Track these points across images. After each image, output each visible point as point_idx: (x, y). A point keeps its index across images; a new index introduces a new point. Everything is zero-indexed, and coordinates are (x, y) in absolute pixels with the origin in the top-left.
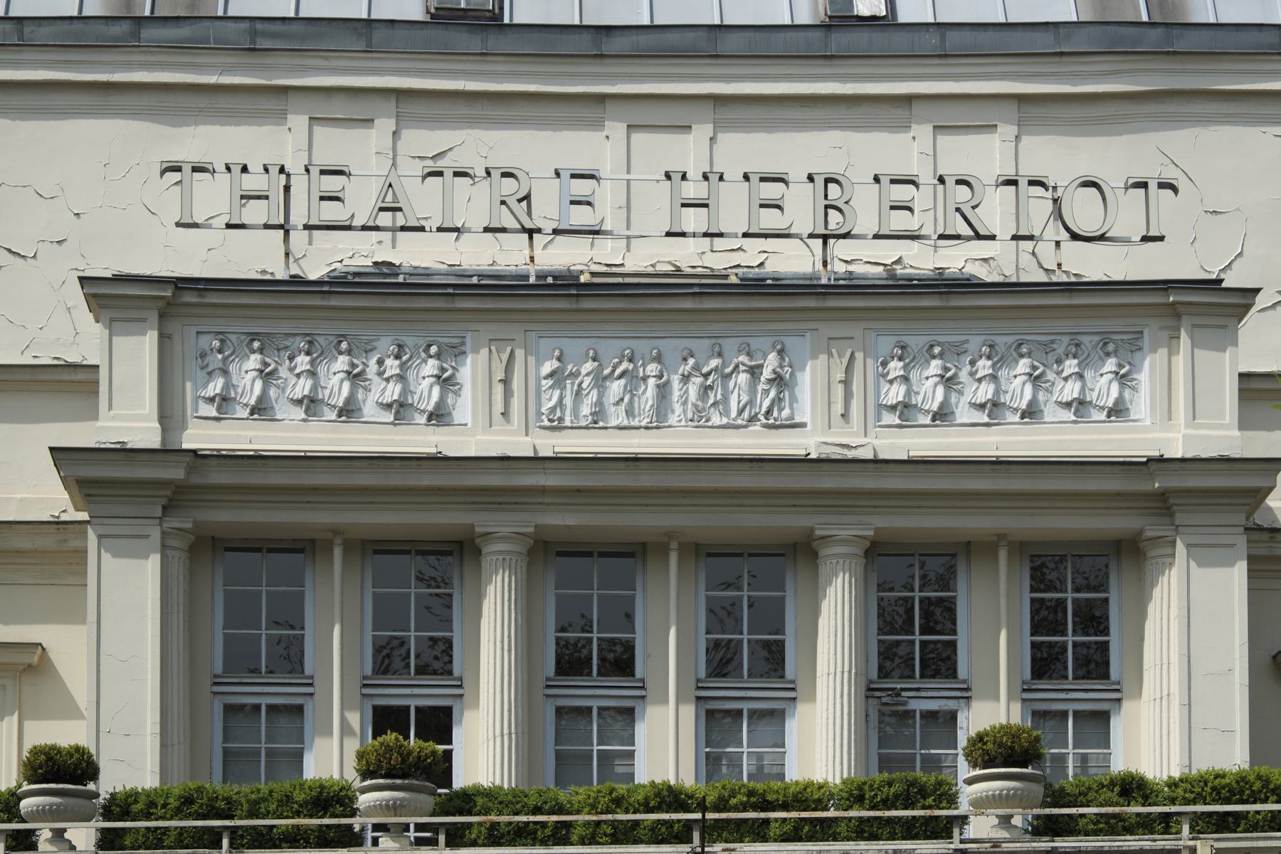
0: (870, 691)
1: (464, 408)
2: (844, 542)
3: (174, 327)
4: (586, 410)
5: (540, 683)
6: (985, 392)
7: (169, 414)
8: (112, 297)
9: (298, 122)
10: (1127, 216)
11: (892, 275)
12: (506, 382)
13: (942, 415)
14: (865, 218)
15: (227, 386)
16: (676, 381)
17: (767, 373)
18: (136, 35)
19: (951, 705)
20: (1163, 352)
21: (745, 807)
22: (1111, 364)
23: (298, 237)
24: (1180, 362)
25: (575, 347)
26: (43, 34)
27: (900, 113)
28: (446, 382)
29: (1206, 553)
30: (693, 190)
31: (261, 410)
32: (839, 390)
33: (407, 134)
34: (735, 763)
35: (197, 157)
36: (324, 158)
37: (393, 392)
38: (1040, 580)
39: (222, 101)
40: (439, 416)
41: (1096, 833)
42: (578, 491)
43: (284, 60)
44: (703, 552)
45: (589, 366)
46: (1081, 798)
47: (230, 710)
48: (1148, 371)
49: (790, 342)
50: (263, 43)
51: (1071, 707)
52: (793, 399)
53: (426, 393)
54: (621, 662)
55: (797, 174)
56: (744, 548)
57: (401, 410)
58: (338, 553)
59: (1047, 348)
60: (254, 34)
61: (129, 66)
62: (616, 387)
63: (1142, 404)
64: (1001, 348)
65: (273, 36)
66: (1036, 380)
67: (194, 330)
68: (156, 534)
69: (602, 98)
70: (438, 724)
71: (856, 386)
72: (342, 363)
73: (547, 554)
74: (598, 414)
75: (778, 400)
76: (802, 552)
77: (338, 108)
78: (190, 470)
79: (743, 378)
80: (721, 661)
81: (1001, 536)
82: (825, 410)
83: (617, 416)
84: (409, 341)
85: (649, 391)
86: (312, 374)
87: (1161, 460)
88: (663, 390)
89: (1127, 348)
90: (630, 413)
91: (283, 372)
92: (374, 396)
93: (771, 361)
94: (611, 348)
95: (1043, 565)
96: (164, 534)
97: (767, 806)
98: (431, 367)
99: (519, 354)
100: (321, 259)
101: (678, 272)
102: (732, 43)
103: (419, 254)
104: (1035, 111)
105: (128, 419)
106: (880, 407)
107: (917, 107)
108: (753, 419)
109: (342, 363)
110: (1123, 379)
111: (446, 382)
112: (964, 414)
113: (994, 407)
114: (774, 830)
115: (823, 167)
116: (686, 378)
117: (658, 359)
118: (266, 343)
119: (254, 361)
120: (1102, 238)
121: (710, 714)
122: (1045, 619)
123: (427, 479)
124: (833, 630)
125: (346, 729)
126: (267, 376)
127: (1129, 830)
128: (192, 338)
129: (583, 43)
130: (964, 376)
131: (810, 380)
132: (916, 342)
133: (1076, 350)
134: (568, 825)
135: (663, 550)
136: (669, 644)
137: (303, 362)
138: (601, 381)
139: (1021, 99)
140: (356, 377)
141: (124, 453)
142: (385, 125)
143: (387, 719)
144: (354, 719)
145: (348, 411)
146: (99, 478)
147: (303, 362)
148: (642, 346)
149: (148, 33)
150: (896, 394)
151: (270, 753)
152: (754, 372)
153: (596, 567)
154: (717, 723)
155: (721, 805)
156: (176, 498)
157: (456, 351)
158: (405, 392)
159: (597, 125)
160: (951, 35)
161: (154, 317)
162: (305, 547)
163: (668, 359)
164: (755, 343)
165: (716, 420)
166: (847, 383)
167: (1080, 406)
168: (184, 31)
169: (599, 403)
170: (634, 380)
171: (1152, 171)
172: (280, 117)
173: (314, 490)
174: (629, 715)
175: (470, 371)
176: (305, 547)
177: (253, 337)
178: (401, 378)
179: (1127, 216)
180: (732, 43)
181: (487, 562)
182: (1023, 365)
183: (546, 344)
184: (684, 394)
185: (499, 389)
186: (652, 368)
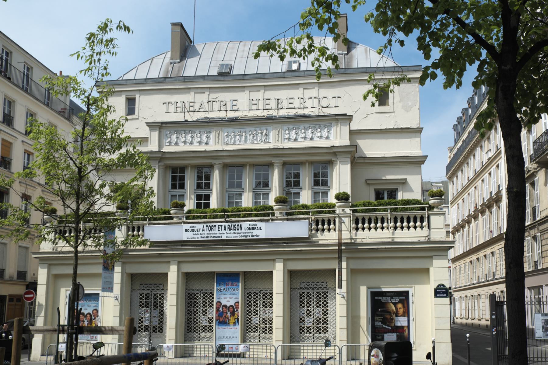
0: (284, 189)
1: (211, 142)
2: (277, 163)
3: (162, 130)
4: (232, 141)
5: (225, 189)
6: (303, 135)
7: (160, 145)
8: (152, 126)
9: (192, 93)
10: (333, 103)
11: (295, 115)
12: (218, 137)
13: (296, 140)
14: (285, 104)
15: (171, 140)
16: (248, 136)
17: (264, 134)
19: (299, 191)
20: (335, 127)
21: (236, 212)
22: (326, 129)
23: (187, 113)
24: (339, 129)
25: (230, 130)
26: (238, 78)
27: (297, 86)
28: (208, 138)
29: (343, 163)
30: (254, 102)
31: (176, 144)
32: (277, 136)
33: (211, 95)
34: (319, 201)
35: (169, 101)
36: (266, 97)
37: (199, 140)
39: (179, 91)
40: (207, 144)
41: (298, 215)
42: (230, 156)
43: (189, 83)
44: (253, 165)
45: (233, 134)
46: (295, 209)
47: (172, 195)
48: (333, 130)
49: (268, 128)
52: (269, 138)
53: (204, 139)
54: (297, 184)
55: (273, 99)
56: (259, 164)
57: (200, 143)
59: (315, 127)
60: (185, 79)
61: (164, 86)
62: (238, 137)
63: (332, 136)
64: (306, 128)
66: (312, 133)
69: (245, 87)
70: (207, 197)
71: (280, 135)
72: (190, 135)
73: (225, 166)
74: (235, 142)
75: (266, 138)
76: (270, 165)
77: (199, 91)
78: (163, 155)
79: (260, 135)
80: (316, 183)
81: (307, 161)
82: (275, 140)
83: (238, 142)
84: (202, 131)
85: (243, 138)
86: (185, 137)
87: (334, 146)
88: (246, 137)
89: (329, 126)
90: (240, 142)
91: (180, 137)
93: (265, 132)
94: (237, 130)
95: (199, 168)
96: (159, 166)
97: (240, 211)
98: (205, 135)
99: (221, 132)
100: (192, 117)
101: (258, 116)
102: (267, 76)
103: (211, 115)
104: (213, 90)
106: (284, 139)
107: (191, 90)
108: (262, 142)
109: (190, 135)
110: (328, 132)
111: (208, 138)
112: (300, 139)
113: (305, 138)
114: (208, 217)
115: (277, 97)
116: (250, 135)
117: (245, 132)
118: (177, 132)
119: (175, 135)
120: (327, 107)
121: (255, 194)
122: (199, 178)
123: (203, 155)
124: (276, 179)
125: (190, 198)
126: (177, 138)
127: (303, 214)
128: (164, 132)
129: (241, 77)
130: (299, 133)
131: (272, 134)
132: (291, 127)
133: (320, 127)
134: (206, 215)
135: (246, 165)
136: (306, 179)
137: (183, 135)
138: (235, 136)
139: (140, 90)
140: (192, 137)
141: (152, 152)
142: (207, 93)
143: (199, 197)
144: (193, 197)
145: (191, 143)
147: (183, 135)
148: (242, 130)
149: (167, 80)
150: (287, 136)
152: (262, 133)
154: (256, 196)
155: (232, 211)
156: (161, 160)
157: (210, 132)
158: (201, 139)
159: (244, 91)
160: (306, 73)
161: (158, 129)
162: (242, 166)
163: (247, 132)
164: (262, 128)
165: (255, 142)
166: (278, 135)
167: (321, 137)
168: (173, 79)
169: (235, 140)
170: (241, 136)
171: (337, 95)
172: (189, 93)
173: (184, 157)
174: (241, 195)
175: (212, 135)
176: (242, 166)
177: (175, 131)
178: (200, 137)
179: (333, 103)
180: (267, 76)
181: (275, 167)
182: (310, 130)
183: (225, 130)
184: (249, 138)
185: (217, 138)
186: (244, 134)
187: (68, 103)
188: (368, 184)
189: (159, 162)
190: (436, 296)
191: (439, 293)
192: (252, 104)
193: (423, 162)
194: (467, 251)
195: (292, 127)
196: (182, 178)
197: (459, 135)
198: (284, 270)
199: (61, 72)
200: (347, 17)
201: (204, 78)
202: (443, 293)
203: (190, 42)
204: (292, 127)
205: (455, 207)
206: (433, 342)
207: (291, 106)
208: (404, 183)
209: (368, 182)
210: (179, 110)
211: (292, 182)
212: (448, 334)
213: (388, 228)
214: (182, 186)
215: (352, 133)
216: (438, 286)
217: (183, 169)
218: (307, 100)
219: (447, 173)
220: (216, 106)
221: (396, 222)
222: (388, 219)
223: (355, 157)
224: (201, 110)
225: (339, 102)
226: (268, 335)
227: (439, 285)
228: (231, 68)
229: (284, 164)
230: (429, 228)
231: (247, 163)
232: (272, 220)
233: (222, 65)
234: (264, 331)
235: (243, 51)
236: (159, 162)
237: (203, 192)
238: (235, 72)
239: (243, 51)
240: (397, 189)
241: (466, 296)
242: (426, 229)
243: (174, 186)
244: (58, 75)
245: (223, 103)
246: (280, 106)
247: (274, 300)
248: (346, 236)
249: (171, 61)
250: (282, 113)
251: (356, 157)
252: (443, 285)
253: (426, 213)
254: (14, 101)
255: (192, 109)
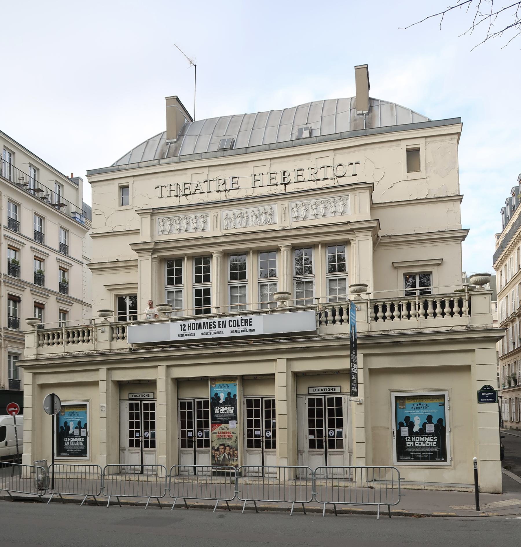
1: (209, 227)
3: (154, 217)
5: (227, 282)
8: (141, 212)
14: (293, 177)
17: (268, 213)
18: (159, 162)
19: (311, 280)
28: (344, 205)
30: (257, 178)
38: (170, 265)
50: (182, 160)
51: (337, 278)
53: (341, 209)
58: (320, 246)
65: (184, 159)
67: (157, 218)
68: (150, 259)
78: (155, 245)
92: (191, 227)
96: (152, 259)
105: (145, 237)
111: (344, 205)
124: (283, 263)
128: (156, 218)
146: (140, 249)
151: (240, 296)
153: (268, 255)
156: (154, 251)
160: (268, 148)
169: (235, 223)
171: (354, 161)
179: (350, 170)
187: (80, 207)
188: (396, 268)
189: (152, 254)
190: (480, 401)
191: (484, 397)
192: (256, 179)
193: (463, 238)
194: (518, 348)
195: (301, 203)
196: (179, 272)
197: (507, 220)
198: (287, 372)
199: (72, 174)
200: (367, 68)
201: (202, 156)
202: (490, 397)
203: (189, 120)
204: (301, 203)
205: (504, 300)
206: (475, 463)
207: (300, 179)
208: (439, 264)
209: (395, 266)
210: (173, 193)
211: (303, 269)
212: (497, 439)
213: (416, 316)
214: (179, 281)
215: (373, 206)
216: (483, 388)
217: (179, 261)
218: (319, 170)
219: (494, 263)
220: (214, 186)
221: (426, 307)
222: (415, 304)
223: (378, 237)
224: (197, 192)
225: (356, 169)
226: (272, 450)
227: (485, 387)
228: (233, 142)
229: (294, 248)
230: (470, 313)
231: (251, 249)
232: (272, 312)
233: (224, 140)
234: (268, 446)
235: (248, 123)
236: (152, 254)
237: (202, 286)
238: (238, 145)
239: (248, 123)
240: (431, 272)
241: (516, 398)
242: (466, 314)
243: (170, 282)
244: (70, 177)
245: (221, 182)
246: (287, 181)
247: (277, 409)
248: (362, 328)
249: (167, 141)
250: (290, 188)
251: (380, 235)
252: (489, 387)
253: (467, 294)
254: (19, 205)
255: (188, 192)
